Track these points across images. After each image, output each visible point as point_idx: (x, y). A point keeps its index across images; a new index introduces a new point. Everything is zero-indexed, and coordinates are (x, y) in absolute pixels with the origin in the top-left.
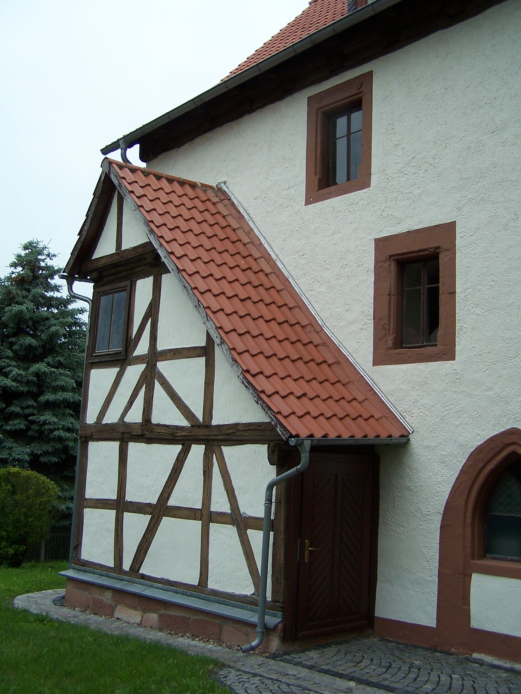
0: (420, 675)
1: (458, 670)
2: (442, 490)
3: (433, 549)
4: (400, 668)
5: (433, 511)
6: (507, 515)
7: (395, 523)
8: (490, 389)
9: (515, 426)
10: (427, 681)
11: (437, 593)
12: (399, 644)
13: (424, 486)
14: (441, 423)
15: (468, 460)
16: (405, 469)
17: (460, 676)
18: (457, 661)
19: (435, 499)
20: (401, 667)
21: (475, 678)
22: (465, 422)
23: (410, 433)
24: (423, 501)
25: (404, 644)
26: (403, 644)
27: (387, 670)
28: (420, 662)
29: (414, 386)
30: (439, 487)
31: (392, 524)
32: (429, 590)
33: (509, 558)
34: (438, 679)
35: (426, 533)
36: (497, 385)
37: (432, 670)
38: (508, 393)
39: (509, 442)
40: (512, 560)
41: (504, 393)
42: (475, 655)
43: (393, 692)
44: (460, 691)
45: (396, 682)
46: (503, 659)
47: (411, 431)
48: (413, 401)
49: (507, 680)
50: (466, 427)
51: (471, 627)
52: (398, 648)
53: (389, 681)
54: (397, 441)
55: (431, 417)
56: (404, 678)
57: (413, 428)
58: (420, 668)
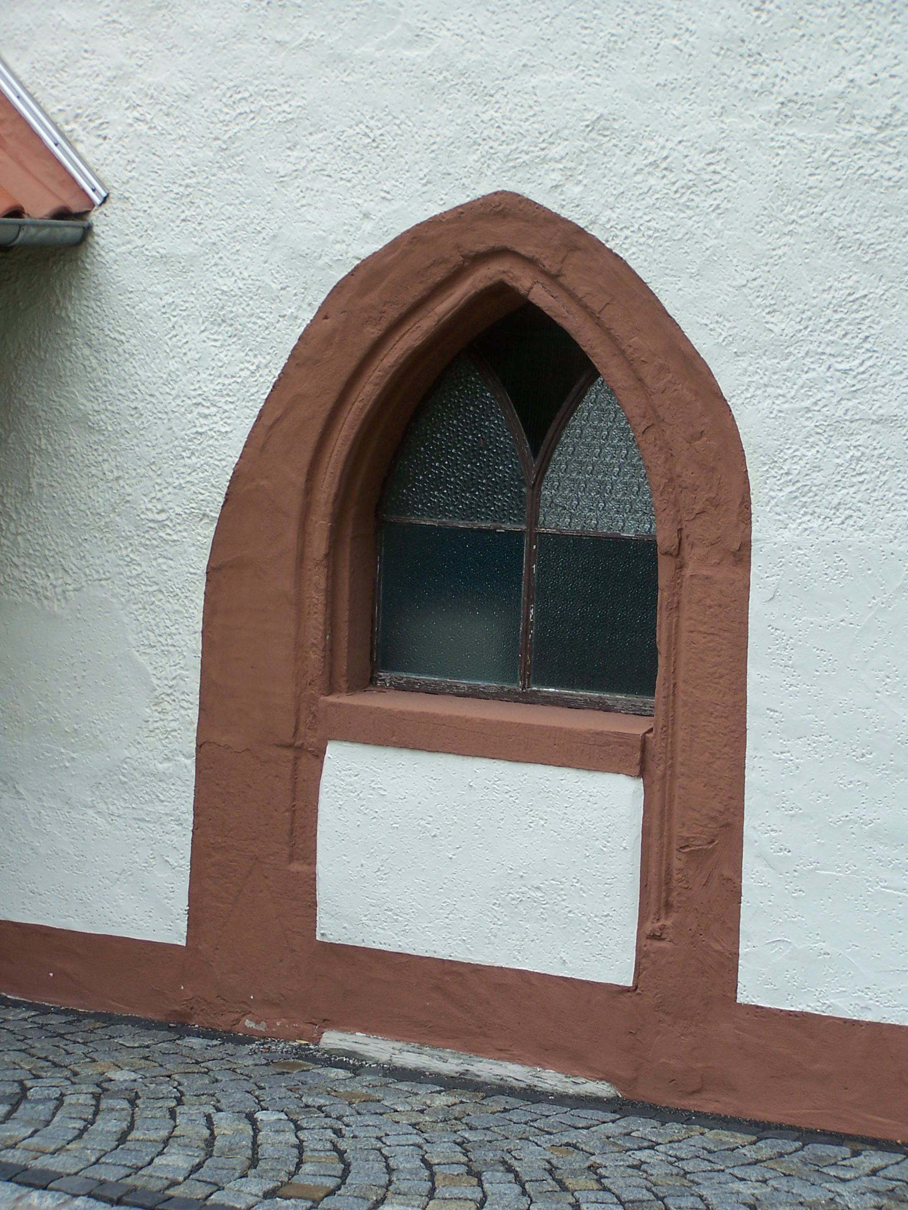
0: (138, 1123)
1: (276, 1096)
2: (217, 427)
3: (181, 653)
4: (60, 1100)
5: (178, 510)
6: (462, 525)
7: (28, 555)
8: (417, 37)
9: (511, 186)
10: (166, 1142)
11: (191, 818)
12: (45, 1011)
13: (147, 413)
14: (221, 167)
15: (323, 313)
16: (69, 347)
17: (283, 1116)
18: (267, 1065)
19: (188, 461)
20: (62, 1095)
21: (339, 1118)
22: (313, 166)
23: (92, 204)
24: (141, 471)
25: (66, 1012)
26: (58, 1012)
27: (15, 1108)
28: (133, 1076)
29: (115, 16)
30: (206, 417)
31: (15, 559)
32: (160, 808)
33: (464, 683)
34: (206, 1133)
35: (152, 594)
36: (448, 24)
37: (180, 1102)
38: (488, 55)
39: (481, 248)
40: (474, 694)
41: (474, 57)
42: (332, 1039)
43: (45, 1188)
44: (292, 1169)
45: (53, 1153)
46: (433, 1047)
47: (99, 194)
48: (109, 74)
49: (448, 1118)
50: (317, 185)
51: (318, 938)
52: (42, 1027)
53: (25, 1149)
54: (45, 232)
55: (180, 143)
56: (79, 1136)
57: (108, 184)
58: (137, 1097)
